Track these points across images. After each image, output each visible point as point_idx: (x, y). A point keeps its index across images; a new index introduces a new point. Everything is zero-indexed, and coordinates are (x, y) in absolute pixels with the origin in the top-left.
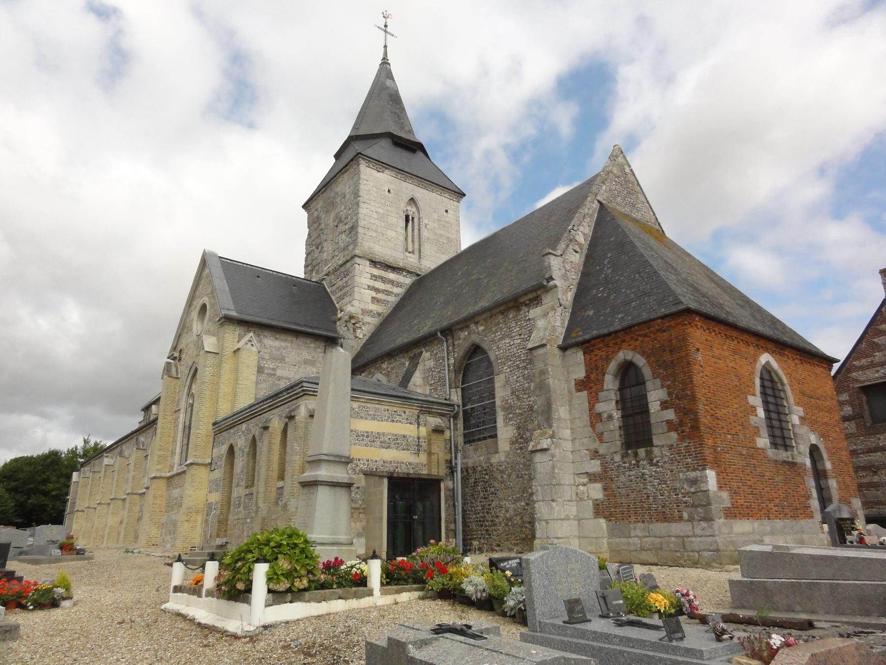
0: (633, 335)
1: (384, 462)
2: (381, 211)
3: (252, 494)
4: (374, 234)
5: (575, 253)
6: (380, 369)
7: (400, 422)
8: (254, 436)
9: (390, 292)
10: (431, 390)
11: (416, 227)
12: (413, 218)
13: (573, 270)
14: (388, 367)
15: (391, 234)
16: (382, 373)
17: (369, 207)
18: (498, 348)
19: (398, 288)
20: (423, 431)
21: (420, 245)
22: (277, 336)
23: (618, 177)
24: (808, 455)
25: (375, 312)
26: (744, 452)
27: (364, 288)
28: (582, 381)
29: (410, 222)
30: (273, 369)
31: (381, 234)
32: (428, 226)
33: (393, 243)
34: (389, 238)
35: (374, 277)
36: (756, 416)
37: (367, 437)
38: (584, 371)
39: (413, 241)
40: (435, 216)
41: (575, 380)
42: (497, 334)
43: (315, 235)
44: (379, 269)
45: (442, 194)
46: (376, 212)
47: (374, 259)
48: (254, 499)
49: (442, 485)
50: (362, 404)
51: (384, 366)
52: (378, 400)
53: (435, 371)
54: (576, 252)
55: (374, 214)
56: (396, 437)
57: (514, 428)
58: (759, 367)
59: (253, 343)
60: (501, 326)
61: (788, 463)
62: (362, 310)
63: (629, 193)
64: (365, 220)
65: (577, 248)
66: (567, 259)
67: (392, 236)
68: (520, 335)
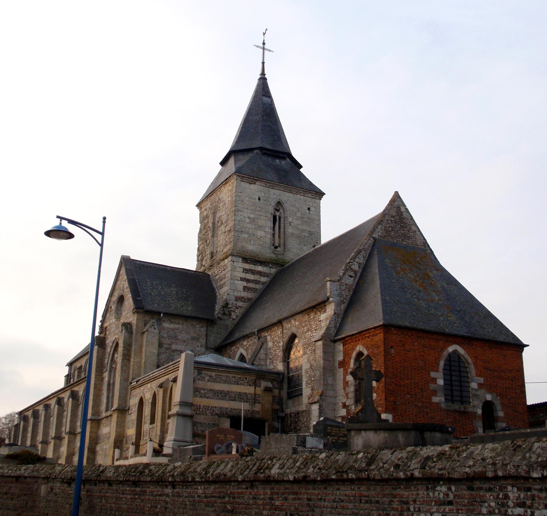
0: (363, 337)
4: (246, 236)
5: (350, 278)
6: (242, 346)
7: (243, 385)
8: (155, 392)
10: (270, 362)
11: (282, 225)
12: (280, 218)
14: (247, 345)
15: (260, 233)
16: (243, 348)
17: (243, 214)
18: (305, 337)
19: (265, 278)
20: (259, 390)
21: (285, 240)
23: (393, 217)
24: (481, 408)
25: (246, 298)
26: (420, 405)
27: (237, 280)
29: (278, 221)
31: (252, 235)
32: (292, 224)
33: (262, 241)
34: (259, 237)
35: (246, 271)
36: (436, 383)
37: (221, 394)
38: (342, 356)
39: (279, 237)
40: (299, 214)
41: (339, 361)
42: (305, 328)
43: (203, 232)
44: (249, 263)
45: (305, 195)
46: (248, 217)
48: (155, 431)
49: (267, 424)
50: (217, 373)
51: (245, 343)
52: (228, 371)
53: (272, 350)
54: (351, 277)
56: (240, 394)
57: (310, 389)
58: (445, 354)
59: (155, 327)
62: (235, 297)
63: (402, 227)
64: (239, 225)
65: (352, 274)
66: (343, 283)
67: (261, 235)
68: (316, 330)
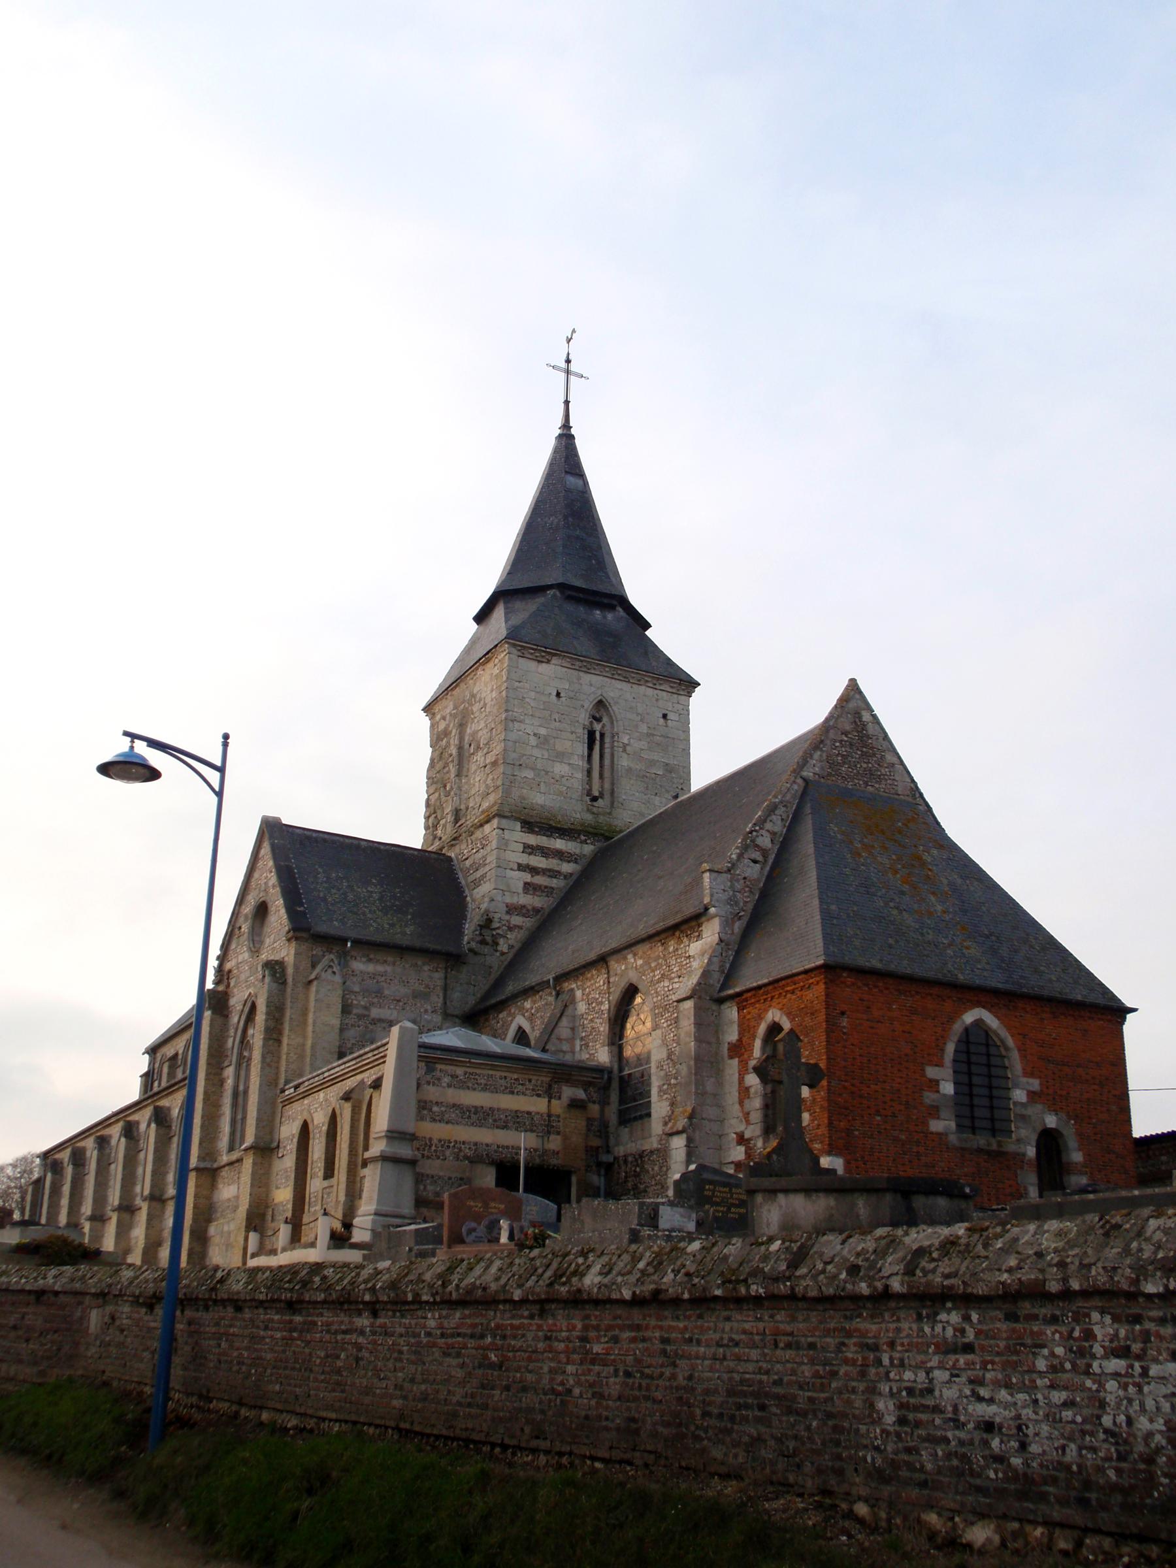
1: (498, 1147)
2: (543, 731)
3: (332, 1186)
4: (529, 774)
5: (752, 864)
9: (557, 871)
10: (581, 1046)
11: (607, 751)
12: (602, 735)
13: (747, 889)
14: (532, 1008)
15: (560, 769)
17: (523, 726)
20: (558, 1106)
21: (613, 784)
22: (372, 956)
23: (845, 733)
24: (1034, 1144)
25: (530, 908)
27: (511, 869)
28: (735, 1045)
29: (598, 743)
30: (366, 1008)
31: (543, 773)
32: (628, 748)
34: (557, 778)
35: (529, 849)
36: (938, 1091)
38: (737, 1033)
39: (601, 776)
40: (644, 728)
44: (537, 833)
45: (657, 687)
46: (535, 735)
47: (529, 819)
49: (574, 1179)
54: (755, 862)
55: (532, 738)
56: (516, 1114)
58: (957, 1028)
59: (335, 970)
60: (660, 961)
61: (989, 1153)
65: (757, 855)
67: (563, 773)
68: (680, 977)
